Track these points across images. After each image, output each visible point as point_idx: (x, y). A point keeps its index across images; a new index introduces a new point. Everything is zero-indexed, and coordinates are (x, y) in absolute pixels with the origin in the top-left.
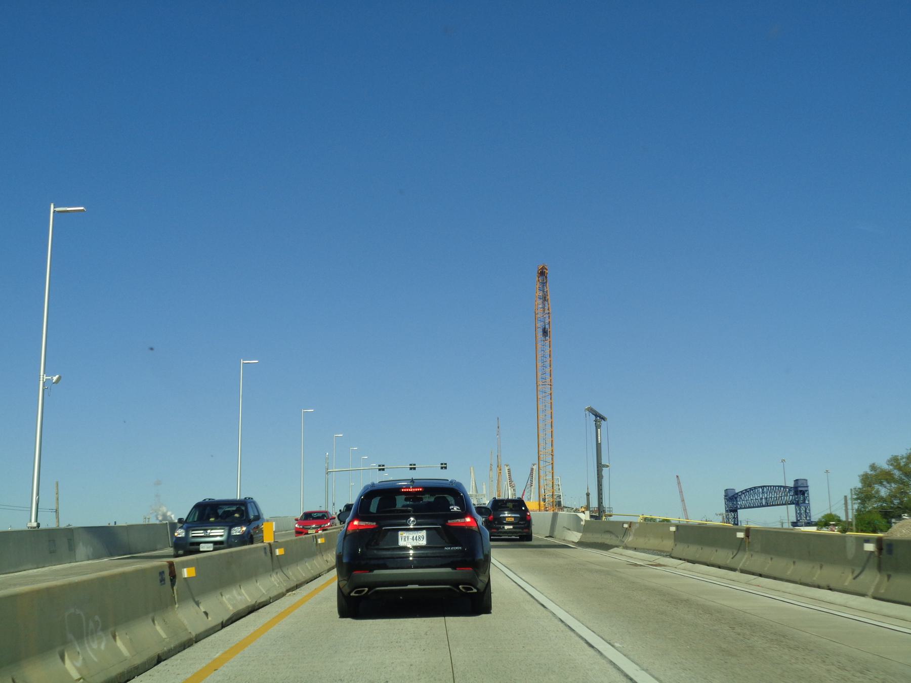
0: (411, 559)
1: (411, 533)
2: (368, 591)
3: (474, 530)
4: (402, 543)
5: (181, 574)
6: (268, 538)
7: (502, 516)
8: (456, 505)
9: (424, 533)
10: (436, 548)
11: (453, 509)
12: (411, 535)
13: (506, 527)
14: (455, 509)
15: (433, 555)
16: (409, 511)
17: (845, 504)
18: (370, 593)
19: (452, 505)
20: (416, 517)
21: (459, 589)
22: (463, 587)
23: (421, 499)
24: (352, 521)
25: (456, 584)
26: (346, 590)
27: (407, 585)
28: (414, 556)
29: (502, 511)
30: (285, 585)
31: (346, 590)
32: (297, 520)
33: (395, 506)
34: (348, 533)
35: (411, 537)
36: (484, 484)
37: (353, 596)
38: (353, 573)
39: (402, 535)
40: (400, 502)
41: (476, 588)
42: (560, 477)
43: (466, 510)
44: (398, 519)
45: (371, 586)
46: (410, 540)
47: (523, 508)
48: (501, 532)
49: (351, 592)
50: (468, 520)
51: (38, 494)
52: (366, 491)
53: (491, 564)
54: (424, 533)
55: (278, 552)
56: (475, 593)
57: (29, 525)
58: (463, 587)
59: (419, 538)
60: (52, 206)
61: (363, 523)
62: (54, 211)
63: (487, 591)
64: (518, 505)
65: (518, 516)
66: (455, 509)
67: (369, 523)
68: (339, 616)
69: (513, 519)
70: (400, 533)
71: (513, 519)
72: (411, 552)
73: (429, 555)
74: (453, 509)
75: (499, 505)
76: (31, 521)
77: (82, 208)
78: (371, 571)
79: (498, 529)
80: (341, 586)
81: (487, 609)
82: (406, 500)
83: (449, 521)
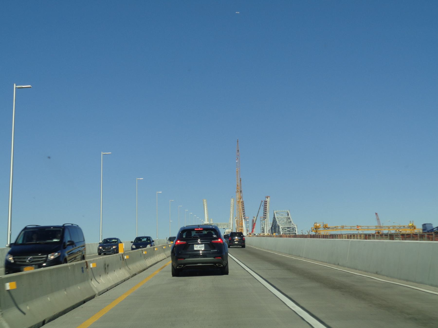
0: (201, 254)
1: (200, 245)
2: (183, 266)
3: (222, 244)
4: (195, 249)
5: (90, 265)
7: (234, 238)
8: (215, 235)
9: (203, 245)
10: (208, 250)
11: (214, 236)
12: (198, 246)
13: (235, 242)
14: (215, 236)
15: (207, 253)
16: (198, 237)
18: (184, 267)
19: (213, 235)
20: (201, 240)
21: (216, 265)
22: (218, 265)
23: (202, 232)
24: (177, 241)
25: (215, 263)
26: (175, 266)
27: (197, 264)
28: (202, 253)
29: (235, 237)
31: (175, 266)
32: (132, 242)
33: (191, 236)
34: (175, 246)
35: (199, 247)
37: (178, 268)
38: (178, 260)
39: (203, 249)
40: (193, 233)
41: (223, 265)
42: (289, 210)
43: (219, 236)
44: (195, 241)
45: (185, 264)
46: (198, 248)
47: (242, 236)
48: (233, 244)
49: (177, 267)
50: (219, 240)
52: (182, 230)
53: (228, 256)
54: (203, 245)
55: (125, 257)
56: (222, 267)
57: (100, 241)
58: (218, 265)
59: (202, 247)
60: (15, 84)
61: (181, 242)
62: (16, 88)
63: (227, 266)
64: (240, 234)
65: (240, 238)
66: (215, 236)
67: (183, 242)
68: (172, 276)
69: (238, 240)
70: (195, 245)
71: (238, 240)
72: (201, 252)
73: (205, 253)
74: (214, 236)
75: (233, 234)
76: (100, 240)
77: (30, 86)
78: (184, 259)
79: (232, 243)
80: (173, 265)
81: (227, 273)
82: (196, 233)
83: (213, 241)
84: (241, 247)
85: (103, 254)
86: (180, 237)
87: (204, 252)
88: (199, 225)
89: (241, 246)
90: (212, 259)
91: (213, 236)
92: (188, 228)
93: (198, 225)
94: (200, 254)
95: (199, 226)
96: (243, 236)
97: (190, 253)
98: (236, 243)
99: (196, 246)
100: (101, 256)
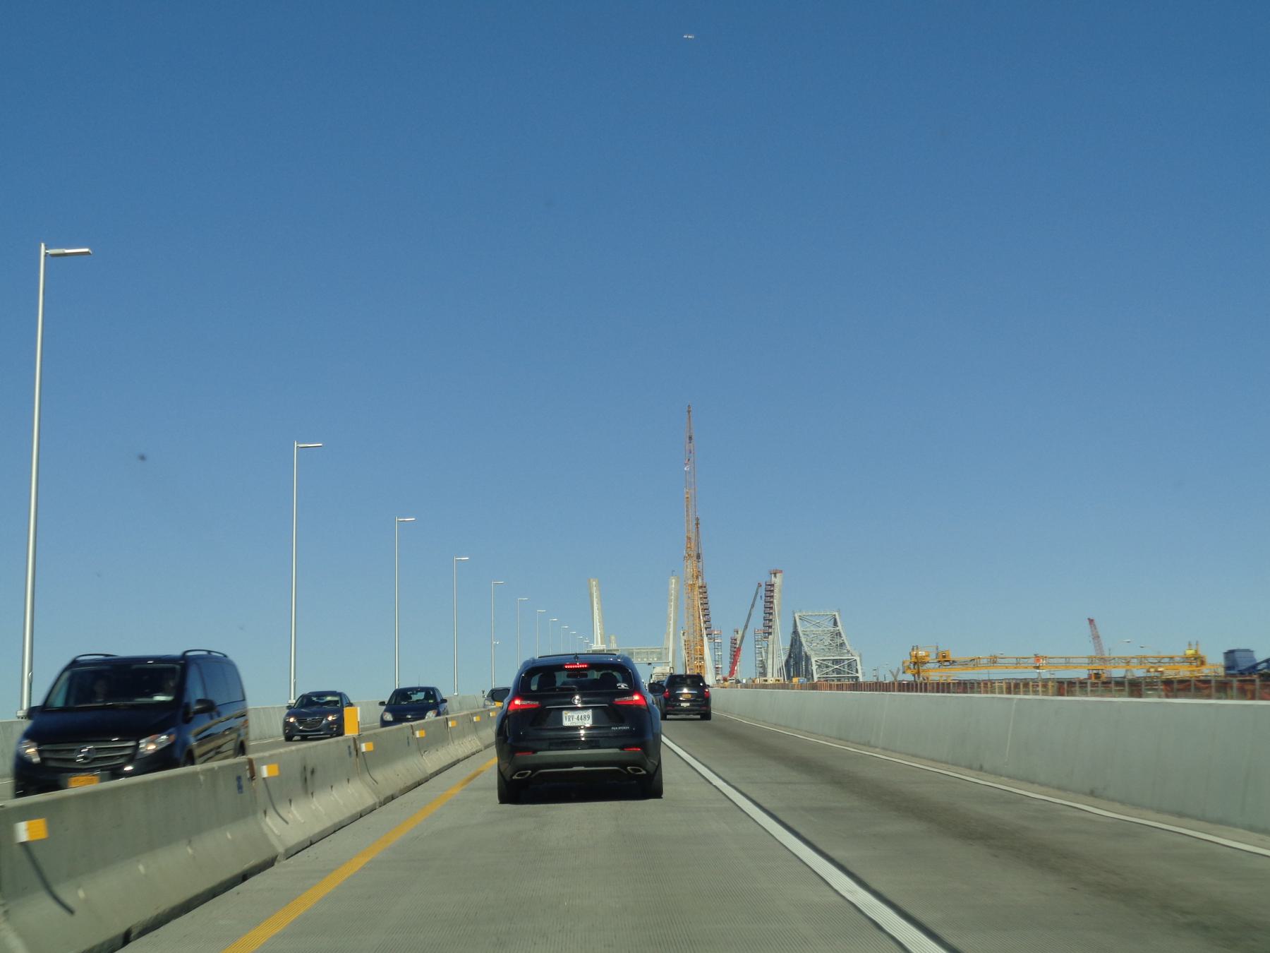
0: (583, 739)
1: (581, 712)
2: (532, 774)
3: (643, 709)
4: (566, 723)
5: (260, 771)
6: (350, 731)
7: (677, 692)
8: (623, 682)
9: (590, 712)
10: (603, 727)
11: (620, 686)
12: (576, 714)
13: (682, 704)
14: (623, 686)
15: (601, 735)
16: (573, 689)
17: (335, 692)
18: (534, 775)
19: (618, 682)
20: (582, 696)
21: (627, 770)
22: (631, 769)
23: (586, 675)
24: (513, 700)
25: (623, 765)
26: (508, 774)
27: (572, 767)
28: (585, 736)
29: (681, 688)
30: (290, 815)
31: (508, 774)
32: (382, 703)
33: (555, 685)
34: (509, 713)
35: (576, 716)
36: (613, 638)
37: (515, 780)
38: (517, 754)
40: (561, 678)
41: (646, 770)
43: (635, 686)
44: (565, 701)
45: (535, 768)
46: (575, 720)
47: (701, 684)
48: (677, 710)
49: (513, 775)
50: (636, 697)
51: (31, 669)
52: (527, 668)
53: (662, 744)
54: (590, 712)
55: (364, 747)
56: (643, 775)
57: (290, 702)
58: (631, 769)
59: (585, 717)
60: (43, 245)
61: (525, 703)
62: (46, 255)
63: (657, 773)
64: (696, 681)
65: (696, 692)
66: (623, 686)
67: (532, 703)
68: (498, 802)
69: (690, 696)
70: (564, 713)
71: (690, 696)
72: (582, 732)
73: (595, 735)
74: (620, 686)
75: (675, 681)
76: (290, 699)
77: (86, 250)
78: (535, 751)
79: (674, 706)
80: (502, 771)
81: (657, 793)
82: (569, 676)
83: (616, 700)
84: (699, 717)
85: (298, 738)
86: (522, 688)
87: (593, 733)
88: (577, 652)
89: (697, 714)
90: (615, 754)
91: (618, 685)
92: (546, 664)
93: (573, 653)
94: (580, 737)
95: (578, 658)
96: (706, 686)
97: (552, 734)
98: (685, 705)
99: (570, 714)
100: (292, 745)
